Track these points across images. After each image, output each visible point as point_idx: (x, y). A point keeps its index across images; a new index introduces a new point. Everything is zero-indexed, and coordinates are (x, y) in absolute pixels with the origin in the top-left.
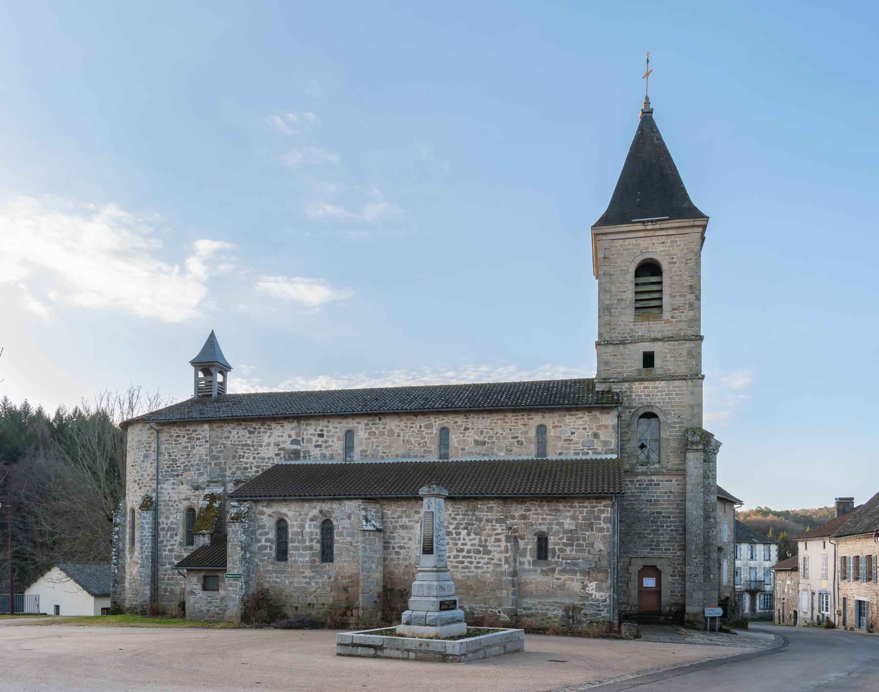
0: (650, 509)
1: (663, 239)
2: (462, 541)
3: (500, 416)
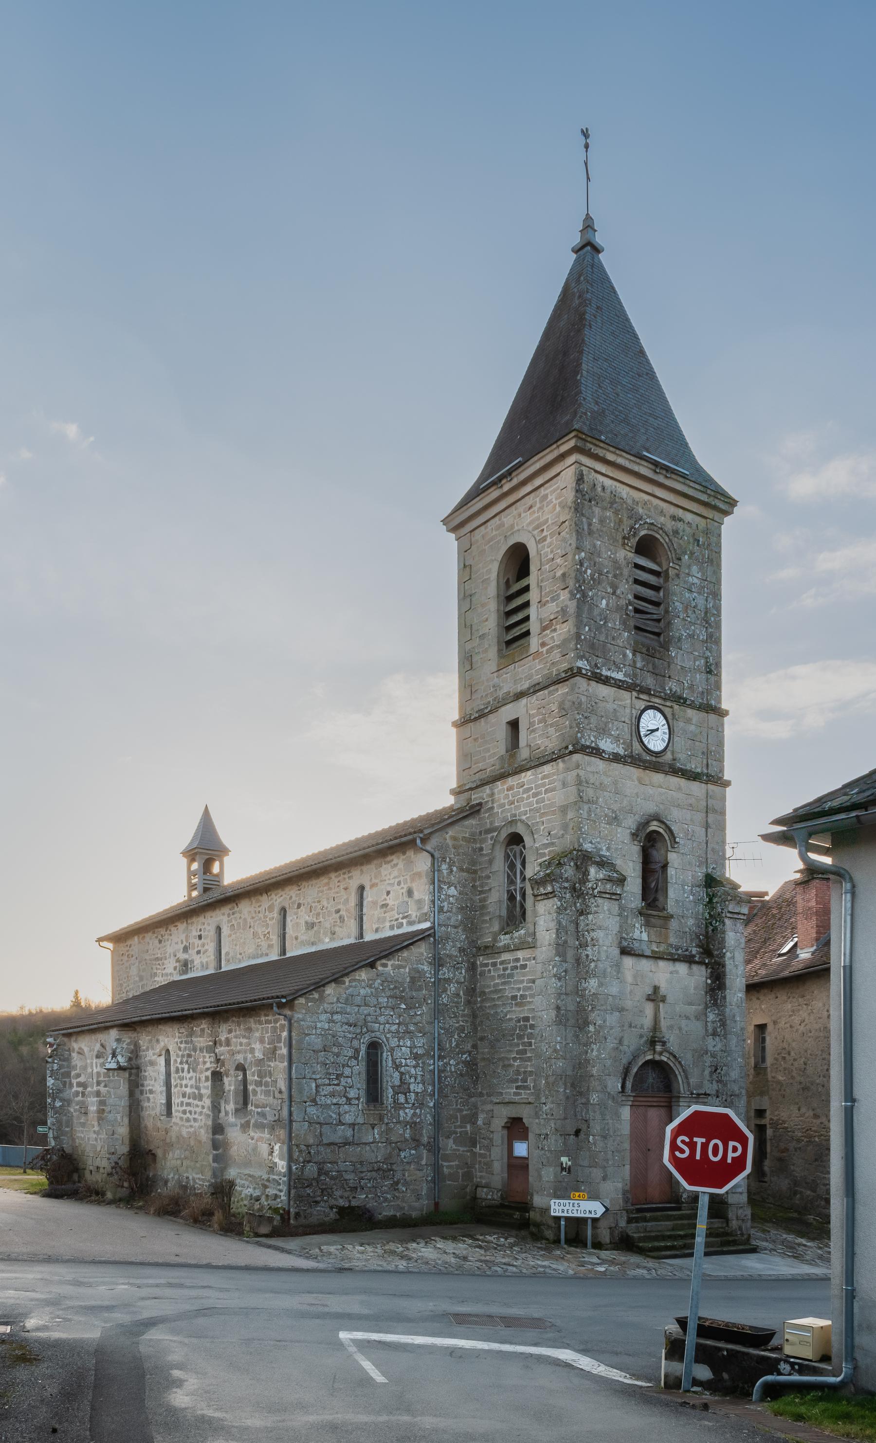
0: (515, 1013)
2: (184, 1082)
3: (324, 880)
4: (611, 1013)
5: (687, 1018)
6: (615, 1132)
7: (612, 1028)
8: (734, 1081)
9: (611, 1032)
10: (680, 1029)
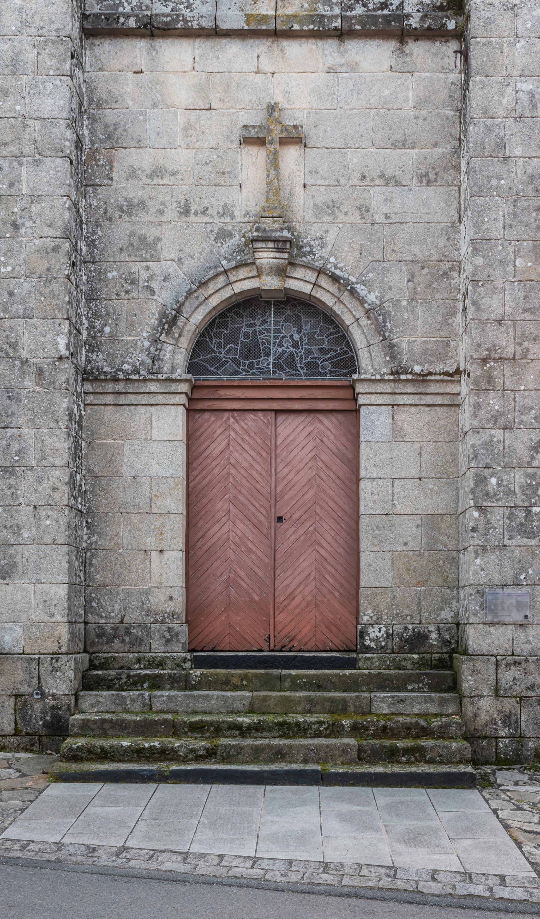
4: (37, 163)
5: (389, 180)
6: (44, 457)
7: (36, 198)
8: (500, 322)
9: (35, 209)
10: (364, 210)
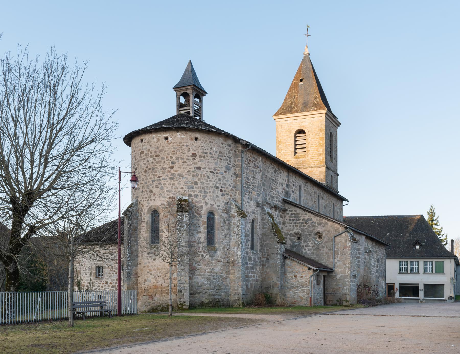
1: (333, 126)
